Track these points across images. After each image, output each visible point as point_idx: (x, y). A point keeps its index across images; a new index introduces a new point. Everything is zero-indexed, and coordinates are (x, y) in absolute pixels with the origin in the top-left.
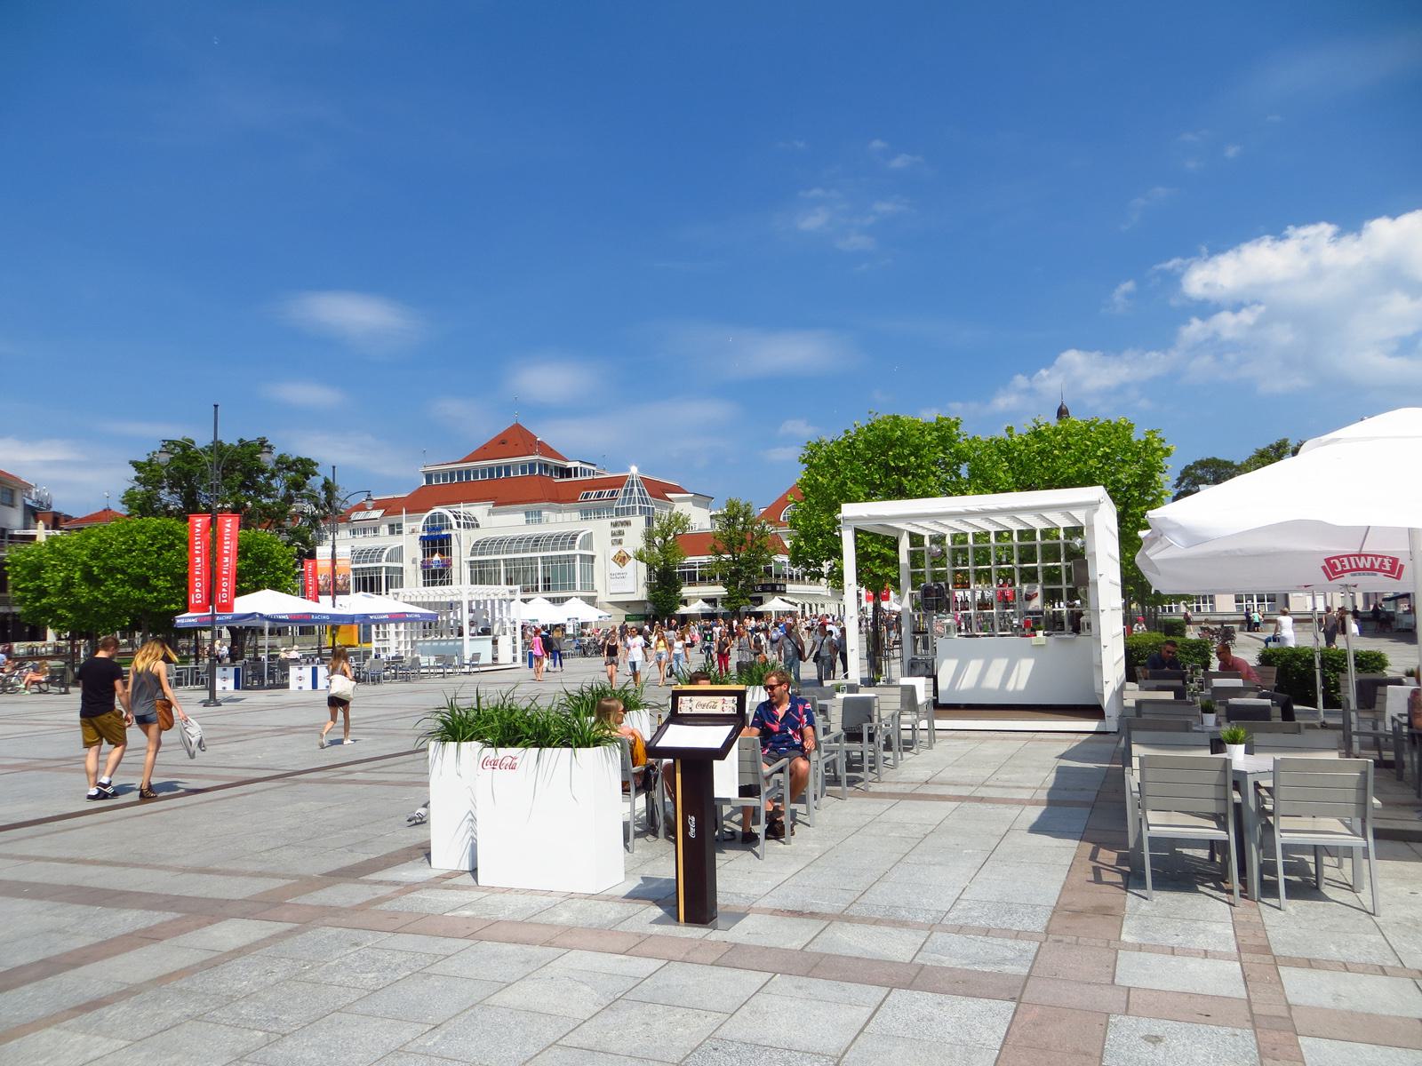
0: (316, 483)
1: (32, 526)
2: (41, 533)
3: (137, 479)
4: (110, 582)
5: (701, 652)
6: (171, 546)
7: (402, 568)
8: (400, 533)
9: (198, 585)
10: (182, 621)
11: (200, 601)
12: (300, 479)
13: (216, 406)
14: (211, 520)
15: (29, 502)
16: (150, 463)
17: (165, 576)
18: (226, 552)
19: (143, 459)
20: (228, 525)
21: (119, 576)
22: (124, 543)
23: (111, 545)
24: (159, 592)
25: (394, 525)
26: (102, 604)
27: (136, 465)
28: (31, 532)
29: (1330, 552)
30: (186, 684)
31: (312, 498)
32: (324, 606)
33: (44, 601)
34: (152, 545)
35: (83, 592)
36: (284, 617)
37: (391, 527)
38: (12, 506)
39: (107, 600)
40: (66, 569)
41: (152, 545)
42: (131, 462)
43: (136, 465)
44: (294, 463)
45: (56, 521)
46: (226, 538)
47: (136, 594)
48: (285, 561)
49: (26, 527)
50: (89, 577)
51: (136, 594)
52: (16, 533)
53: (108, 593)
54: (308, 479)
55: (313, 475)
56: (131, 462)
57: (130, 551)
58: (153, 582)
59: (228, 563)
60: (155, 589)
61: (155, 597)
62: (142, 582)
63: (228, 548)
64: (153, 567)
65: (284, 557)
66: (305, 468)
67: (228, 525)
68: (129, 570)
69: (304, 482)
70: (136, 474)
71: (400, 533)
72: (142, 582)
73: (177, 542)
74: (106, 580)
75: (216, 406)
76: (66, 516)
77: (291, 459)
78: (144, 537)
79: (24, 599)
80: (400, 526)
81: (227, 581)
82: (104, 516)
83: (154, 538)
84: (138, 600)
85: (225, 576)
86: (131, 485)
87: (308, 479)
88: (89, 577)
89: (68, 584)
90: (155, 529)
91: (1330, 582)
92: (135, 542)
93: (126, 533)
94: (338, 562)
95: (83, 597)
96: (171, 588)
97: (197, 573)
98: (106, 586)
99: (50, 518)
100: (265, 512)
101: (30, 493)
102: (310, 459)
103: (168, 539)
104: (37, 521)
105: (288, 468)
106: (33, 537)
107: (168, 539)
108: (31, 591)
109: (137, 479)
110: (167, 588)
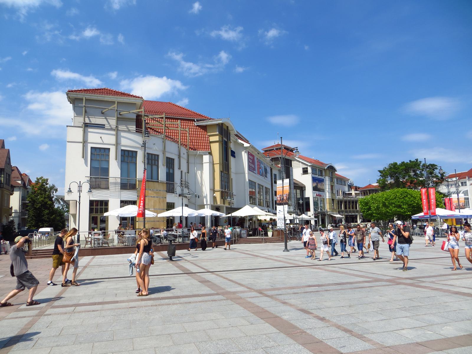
0: (437, 172)
1: (350, 190)
2: (353, 192)
3: (380, 175)
4: (391, 207)
5: (420, 162)
6: (407, 196)
7: (468, 198)
8: (466, 185)
9: (425, 207)
10: (414, 218)
11: (433, 212)
12: (431, 170)
13: (455, 170)
14: (427, 190)
15: (349, 184)
16: (384, 170)
17: (406, 205)
18: (424, 199)
19: (382, 169)
20: (432, 192)
21: (393, 205)
22: (394, 196)
23: (390, 196)
24: (405, 209)
25: (463, 183)
26: (389, 213)
27: (380, 171)
28: (350, 192)
29: (298, 264)
30: (415, 235)
31: (436, 177)
32: (456, 213)
33: (369, 212)
34: (401, 196)
35: (384, 210)
36: (458, 216)
37: (462, 183)
38: (345, 185)
39: (390, 212)
40: (377, 203)
41: (401, 196)
42: (378, 171)
43: (380, 171)
44: (429, 166)
45: (356, 189)
46: (432, 196)
47: (398, 210)
48: (439, 199)
49: (349, 191)
50: (384, 205)
51: (398, 210)
52: (347, 193)
53: (391, 210)
54: (434, 170)
55: (436, 169)
56: (378, 171)
57: (395, 198)
58: (402, 206)
59: (433, 201)
60: (403, 208)
61: (403, 211)
62: (399, 206)
63: (432, 197)
64: (402, 202)
65: (439, 198)
66: (433, 167)
67: (432, 191)
68: (396, 203)
69: (433, 172)
70: (380, 174)
71: (466, 185)
72: (399, 206)
73: (408, 195)
74: (390, 206)
75: (455, 170)
76: (358, 187)
77: (427, 165)
78: (399, 194)
79: (364, 211)
80: (465, 183)
81: (433, 206)
82: (369, 186)
83: (401, 194)
84: (398, 212)
85: (432, 205)
86: (379, 177)
87: (434, 170)
88: (384, 205)
89: (378, 208)
90: (402, 192)
91: (286, 253)
92: (396, 195)
93: (394, 193)
94: (460, 199)
95: (383, 211)
96: (408, 208)
97: (425, 204)
98: (390, 208)
99: (355, 188)
100: (421, 183)
101: (348, 181)
102: (434, 164)
103: (405, 194)
104: (352, 189)
105: (427, 168)
106: (351, 194)
107: (405, 194)
108: (366, 209)
109: (380, 175)
110: (407, 208)
